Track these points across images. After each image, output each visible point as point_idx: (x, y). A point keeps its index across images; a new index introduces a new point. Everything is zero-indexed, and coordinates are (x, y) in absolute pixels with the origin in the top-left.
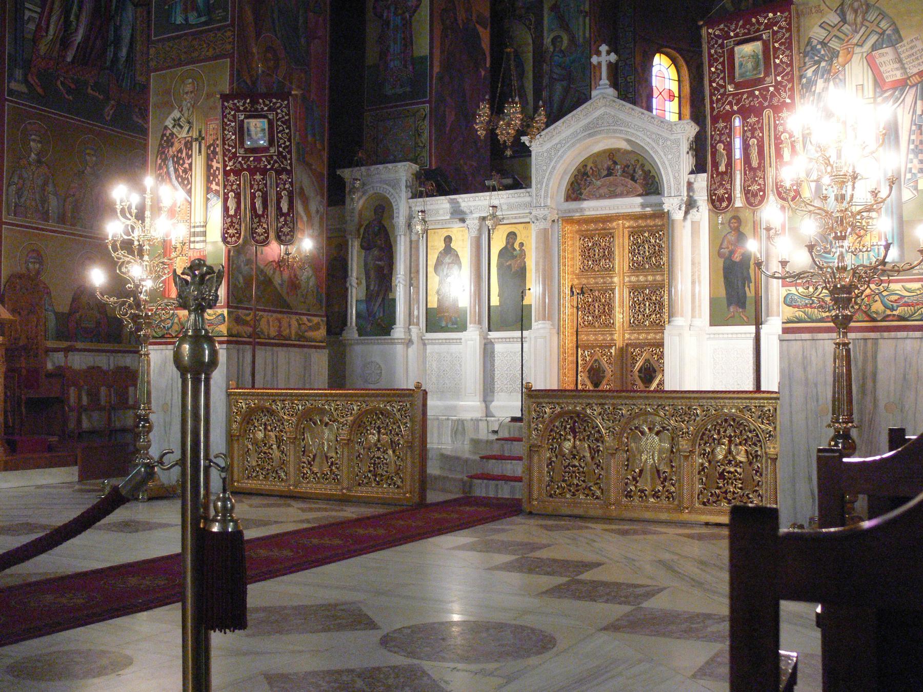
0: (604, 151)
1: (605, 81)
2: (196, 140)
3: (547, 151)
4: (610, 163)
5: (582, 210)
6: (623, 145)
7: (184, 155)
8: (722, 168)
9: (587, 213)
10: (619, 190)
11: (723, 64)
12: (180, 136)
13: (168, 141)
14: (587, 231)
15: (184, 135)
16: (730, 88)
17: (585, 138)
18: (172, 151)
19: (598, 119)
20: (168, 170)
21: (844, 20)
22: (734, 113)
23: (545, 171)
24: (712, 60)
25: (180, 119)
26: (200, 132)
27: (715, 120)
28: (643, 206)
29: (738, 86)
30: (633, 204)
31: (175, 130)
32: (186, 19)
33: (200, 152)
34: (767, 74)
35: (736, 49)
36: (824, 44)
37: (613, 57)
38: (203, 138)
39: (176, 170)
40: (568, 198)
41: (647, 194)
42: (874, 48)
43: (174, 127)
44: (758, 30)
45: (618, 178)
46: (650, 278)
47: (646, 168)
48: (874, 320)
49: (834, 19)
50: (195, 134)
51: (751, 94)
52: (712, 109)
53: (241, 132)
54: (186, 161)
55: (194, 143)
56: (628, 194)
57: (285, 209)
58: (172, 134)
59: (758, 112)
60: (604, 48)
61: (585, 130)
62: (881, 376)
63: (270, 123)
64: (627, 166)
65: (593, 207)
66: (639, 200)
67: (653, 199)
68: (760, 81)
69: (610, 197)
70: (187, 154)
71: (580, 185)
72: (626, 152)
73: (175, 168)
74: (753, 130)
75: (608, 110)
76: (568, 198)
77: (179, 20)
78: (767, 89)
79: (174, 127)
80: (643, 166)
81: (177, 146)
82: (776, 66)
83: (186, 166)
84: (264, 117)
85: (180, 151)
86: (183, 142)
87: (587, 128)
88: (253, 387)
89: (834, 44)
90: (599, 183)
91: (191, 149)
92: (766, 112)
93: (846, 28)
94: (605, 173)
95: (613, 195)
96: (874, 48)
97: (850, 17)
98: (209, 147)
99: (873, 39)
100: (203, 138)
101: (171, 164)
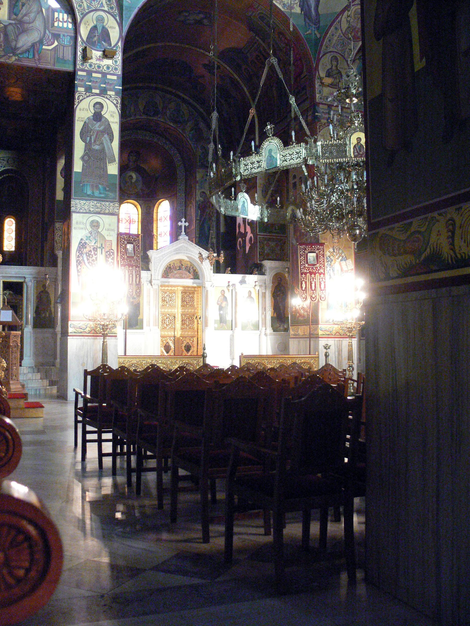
0: (178, 260)
1: (183, 233)
2: (99, 248)
3: (159, 257)
4: (180, 265)
5: (169, 282)
6: (186, 259)
7: (93, 253)
8: (304, 289)
9: (170, 283)
10: (184, 276)
11: (304, 257)
12: (90, 245)
13: (83, 245)
14: (171, 290)
15: (93, 244)
16: (306, 265)
17: (175, 254)
18: (85, 251)
19: (180, 247)
20: (83, 258)
21: (334, 251)
22: (307, 273)
23: (158, 265)
24: (301, 256)
25: (90, 237)
26: (102, 245)
27: (302, 274)
28: (193, 283)
29: (309, 265)
30: (189, 282)
31: (87, 241)
32: (93, 193)
33: (102, 253)
34: (318, 263)
35: (309, 254)
36: (329, 257)
37: (187, 224)
38: (103, 248)
39: (88, 259)
40: (163, 277)
41: (195, 279)
42: (341, 260)
43: (87, 240)
44: (315, 250)
45: (183, 271)
46: (190, 311)
47: (194, 269)
48: (341, 335)
49: (332, 250)
50: (99, 245)
51: (312, 268)
52: (301, 271)
53: (126, 249)
54: (94, 256)
55: (98, 249)
56: (187, 278)
57: (138, 283)
58: (85, 243)
59: (315, 274)
60: (183, 220)
61: (174, 251)
62: (343, 350)
63: (134, 246)
64: (187, 267)
65: (173, 281)
66: (192, 281)
67: (197, 281)
68: (316, 265)
69: (180, 278)
70: (94, 253)
71: (169, 271)
72: (187, 261)
73: (87, 258)
74: (313, 279)
75: (184, 245)
76: (163, 277)
77: (89, 192)
78: (317, 267)
79: (87, 240)
80: (193, 268)
81: (88, 249)
82: (320, 261)
83: (94, 258)
84: (132, 243)
85: (90, 251)
86: (92, 247)
87: (176, 250)
88: (310, 354)
89: (332, 257)
90: (176, 272)
91: (97, 251)
92: (317, 274)
93: (334, 253)
94: (178, 268)
95: (181, 278)
96: (341, 260)
97: (335, 251)
98: (107, 252)
99: (341, 258)
100: (103, 248)
101: (85, 256)
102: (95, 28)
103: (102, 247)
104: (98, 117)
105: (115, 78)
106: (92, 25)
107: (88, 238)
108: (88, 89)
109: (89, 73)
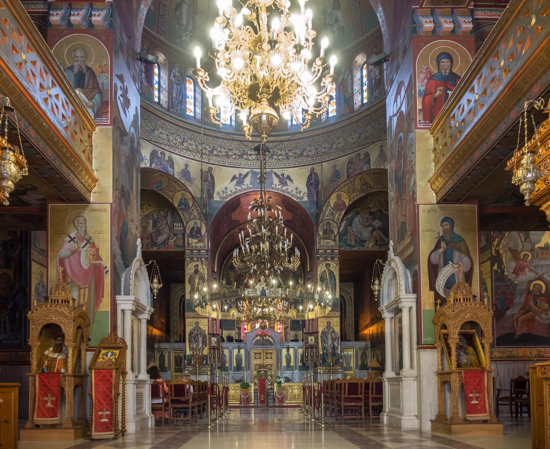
81: (194, 335)
102: (193, 228)
103: (200, 334)
104: (196, 271)
105: (205, 251)
106: (192, 227)
107: (194, 330)
108: (192, 259)
109: (192, 251)
